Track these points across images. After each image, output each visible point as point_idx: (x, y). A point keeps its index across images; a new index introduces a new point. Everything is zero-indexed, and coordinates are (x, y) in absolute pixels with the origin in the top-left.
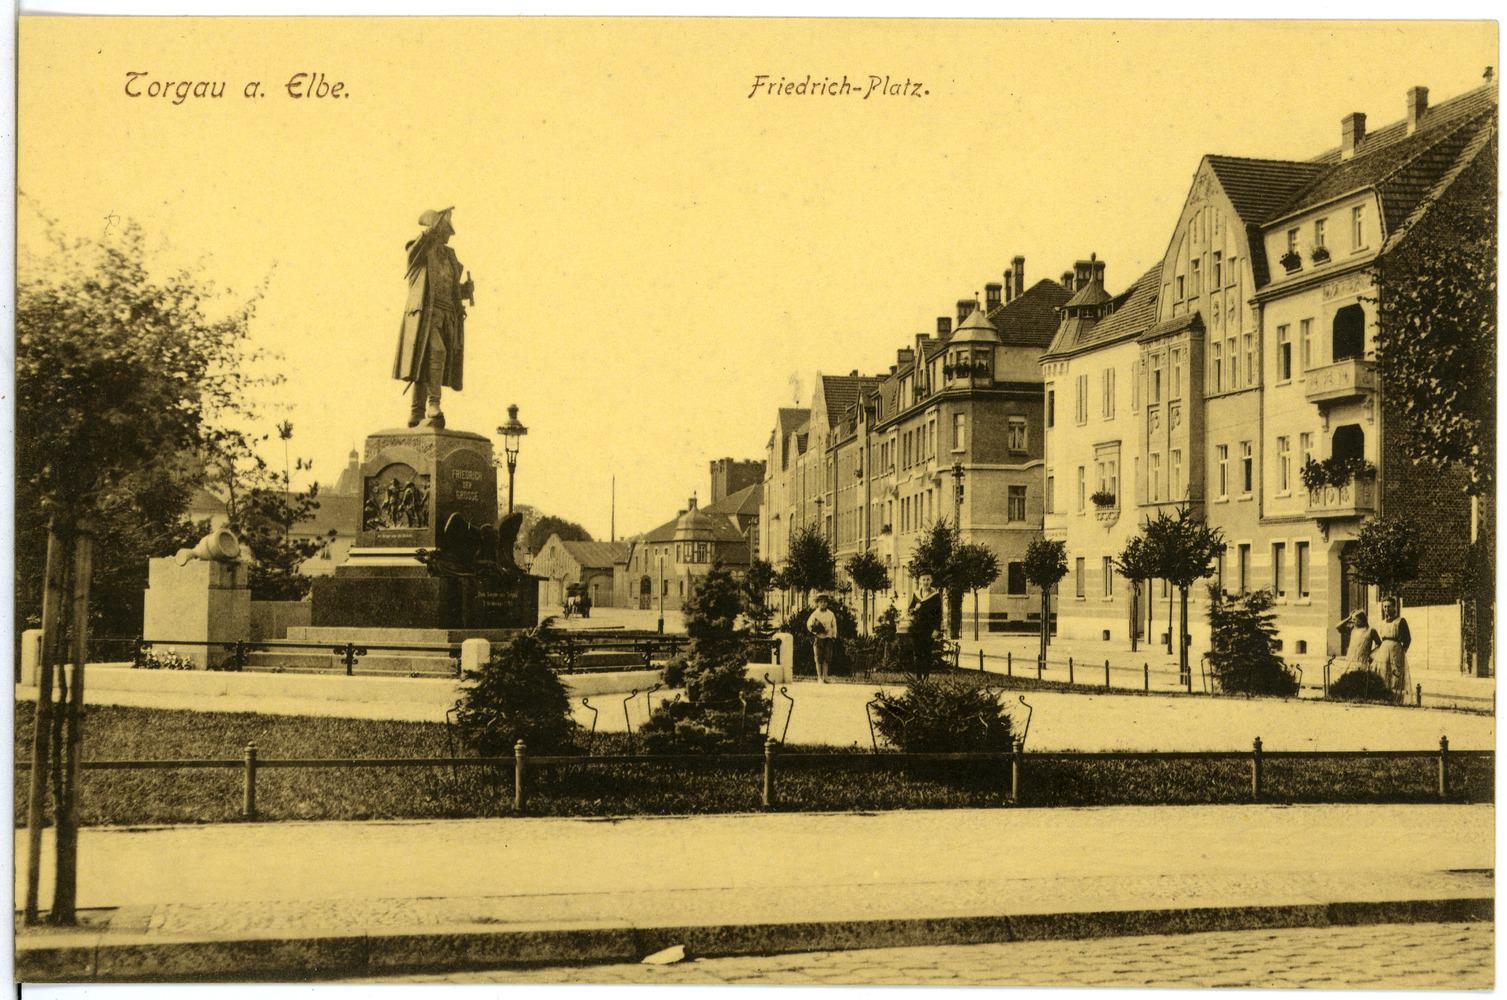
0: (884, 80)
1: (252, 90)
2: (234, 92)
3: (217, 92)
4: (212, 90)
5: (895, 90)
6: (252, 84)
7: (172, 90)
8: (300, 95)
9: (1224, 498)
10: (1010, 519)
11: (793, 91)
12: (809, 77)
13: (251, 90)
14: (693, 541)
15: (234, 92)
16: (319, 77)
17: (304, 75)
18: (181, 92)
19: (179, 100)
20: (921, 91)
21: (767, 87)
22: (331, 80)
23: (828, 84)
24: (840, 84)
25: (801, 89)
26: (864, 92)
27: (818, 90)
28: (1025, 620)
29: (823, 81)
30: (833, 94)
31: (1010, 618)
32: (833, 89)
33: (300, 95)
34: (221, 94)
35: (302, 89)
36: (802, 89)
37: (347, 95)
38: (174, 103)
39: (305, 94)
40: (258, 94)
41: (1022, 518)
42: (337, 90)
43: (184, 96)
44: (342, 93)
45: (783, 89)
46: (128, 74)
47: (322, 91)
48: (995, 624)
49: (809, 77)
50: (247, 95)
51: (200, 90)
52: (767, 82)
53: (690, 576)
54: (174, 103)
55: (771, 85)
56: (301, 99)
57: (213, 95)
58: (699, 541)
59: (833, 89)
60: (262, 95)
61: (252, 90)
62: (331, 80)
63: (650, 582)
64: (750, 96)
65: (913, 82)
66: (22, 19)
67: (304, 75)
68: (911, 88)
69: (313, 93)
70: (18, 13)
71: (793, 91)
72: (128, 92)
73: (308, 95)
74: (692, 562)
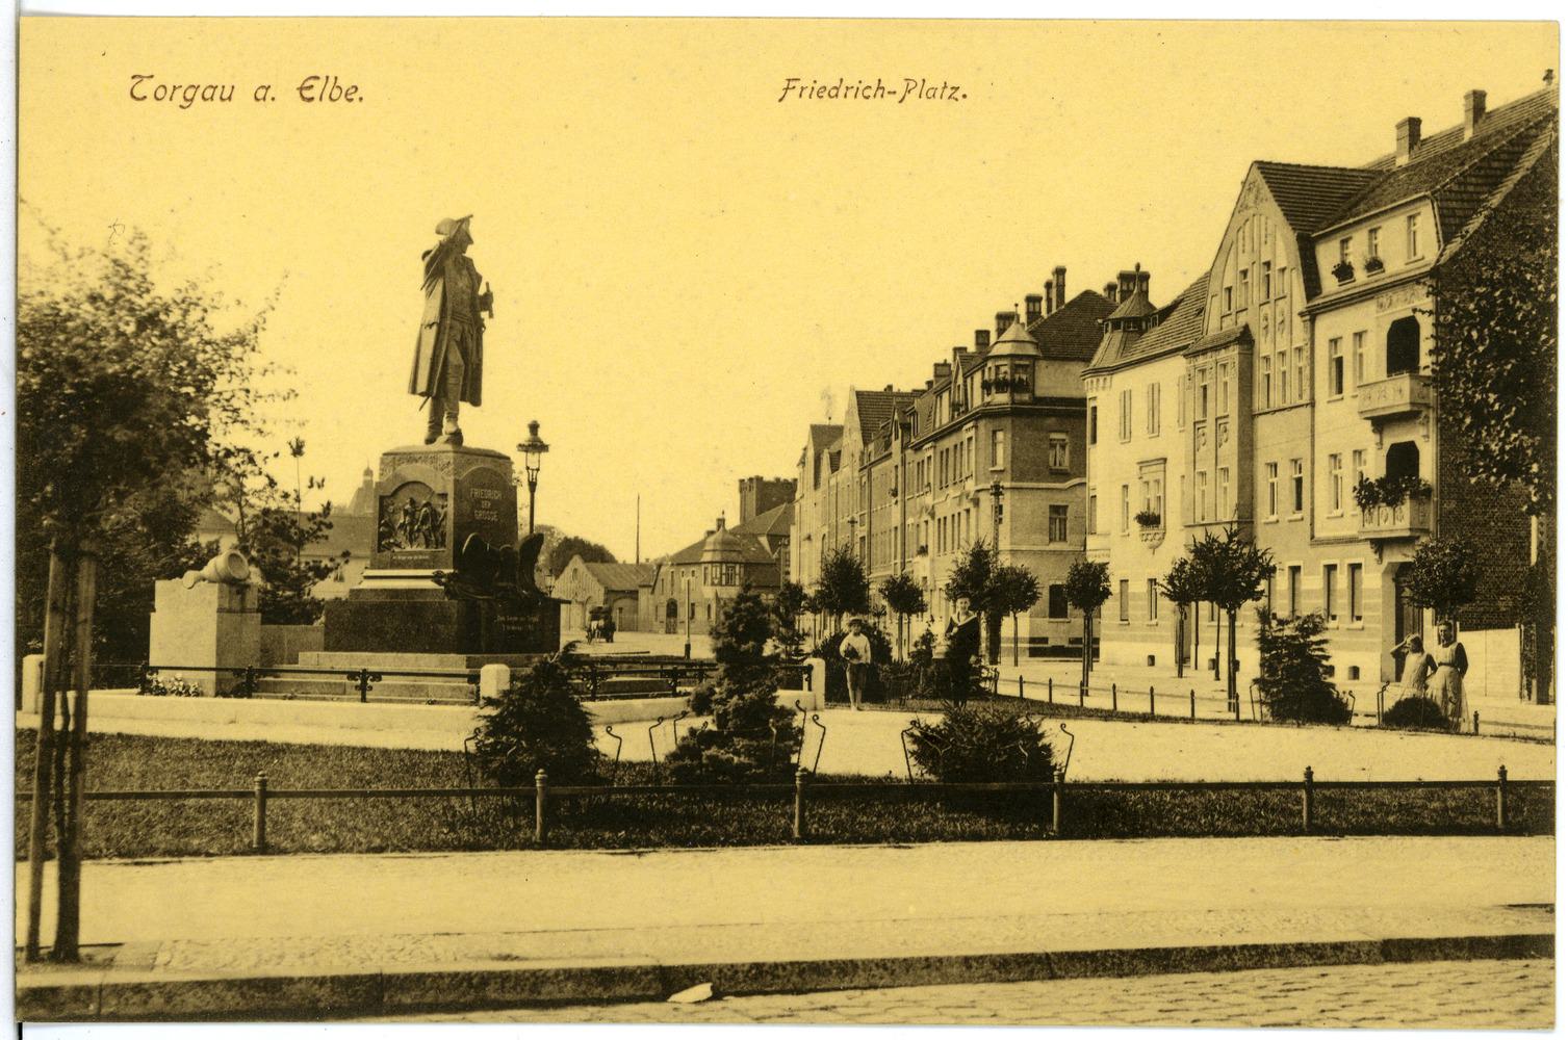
0: (920, 83)
1: (262, 94)
2: (243, 96)
3: (225, 96)
4: (220, 94)
5: (931, 94)
6: (263, 87)
7: (179, 94)
8: (312, 99)
9: (1273, 518)
10: (1051, 540)
11: (825, 94)
12: (841, 80)
13: (261, 94)
14: (721, 563)
15: (243, 96)
16: (332, 80)
17: (317, 78)
18: (189, 96)
19: (186, 104)
20: (958, 95)
21: (798, 90)
22: (345, 84)
23: (862, 87)
24: (874, 87)
25: (833, 93)
26: (899, 96)
27: (851, 93)
28: (1066, 645)
29: (856, 85)
30: (867, 98)
31: (1051, 643)
32: (867, 93)
33: (312, 99)
34: (230, 98)
35: (315, 93)
36: (834, 92)
37: (361, 99)
38: (181, 107)
39: (317, 97)
40: (268, 98)
41: (1063, 539)
42: (350, 94)
43: (192, 100)
44: (355, 97)
45: (815, 93)
46: (133, 77)
47: (335, 95)
48: (1035, 648)
49: (841, 80)
50: (257, 99)
51: (208, 94)
52: (798, 85)
53: (718, 599)
54: (181, 107)
55: (802, 88)
56: (313, 103)
57: (221, 99)
58: (727, 563)
59: (867, 93)
60: (273, 99)
61: (262, 94)
62: (345, 84)
63: (676, 606)
64: (780, 100)
65: (949, 85)
66: (22, 19)
67: (317, 78)
68: (948, 92)
69: (326, 96)
70: (19, 14)
71: (825, 94)
72: (133, 96)
73: (321, 99)
74: (720, 584)
